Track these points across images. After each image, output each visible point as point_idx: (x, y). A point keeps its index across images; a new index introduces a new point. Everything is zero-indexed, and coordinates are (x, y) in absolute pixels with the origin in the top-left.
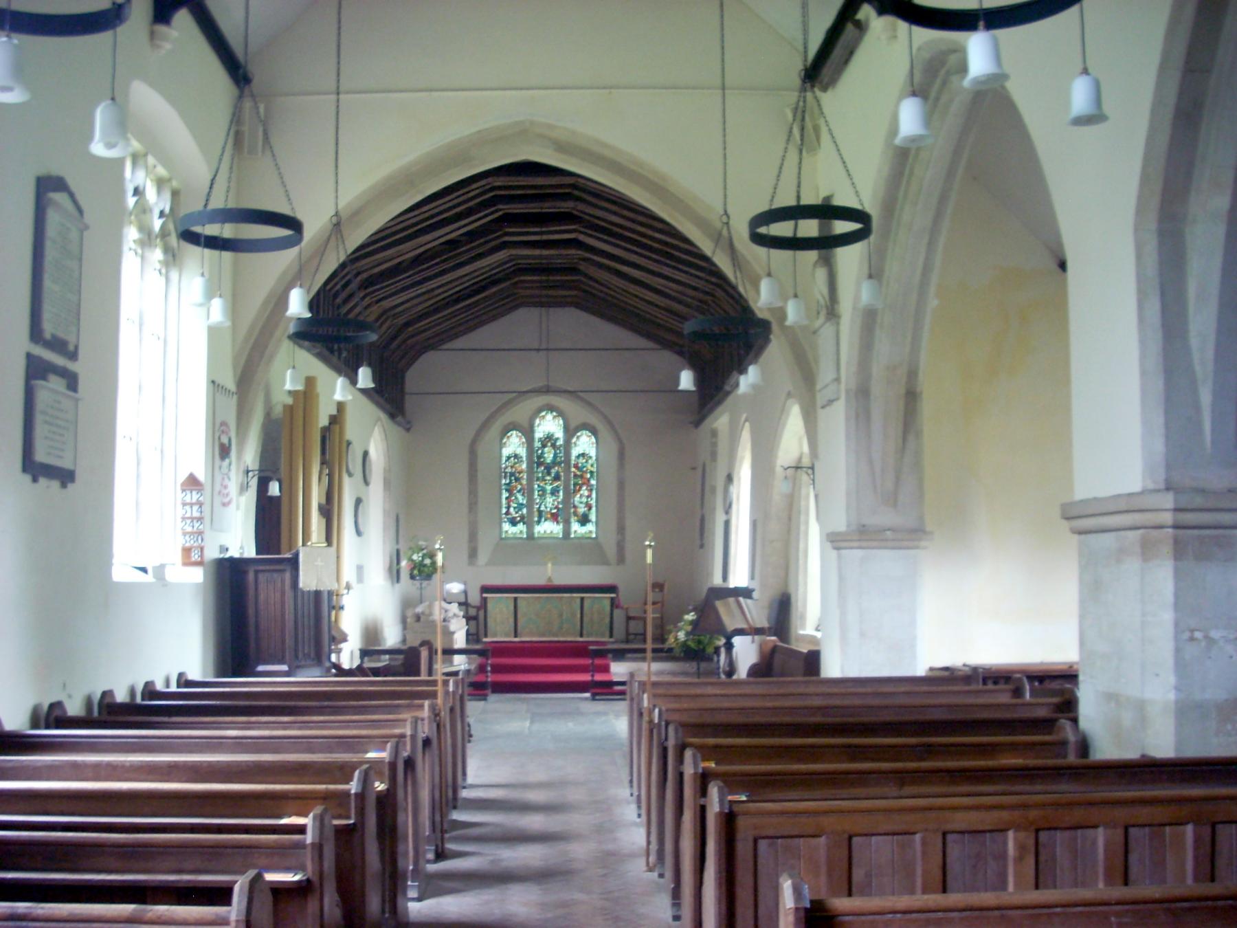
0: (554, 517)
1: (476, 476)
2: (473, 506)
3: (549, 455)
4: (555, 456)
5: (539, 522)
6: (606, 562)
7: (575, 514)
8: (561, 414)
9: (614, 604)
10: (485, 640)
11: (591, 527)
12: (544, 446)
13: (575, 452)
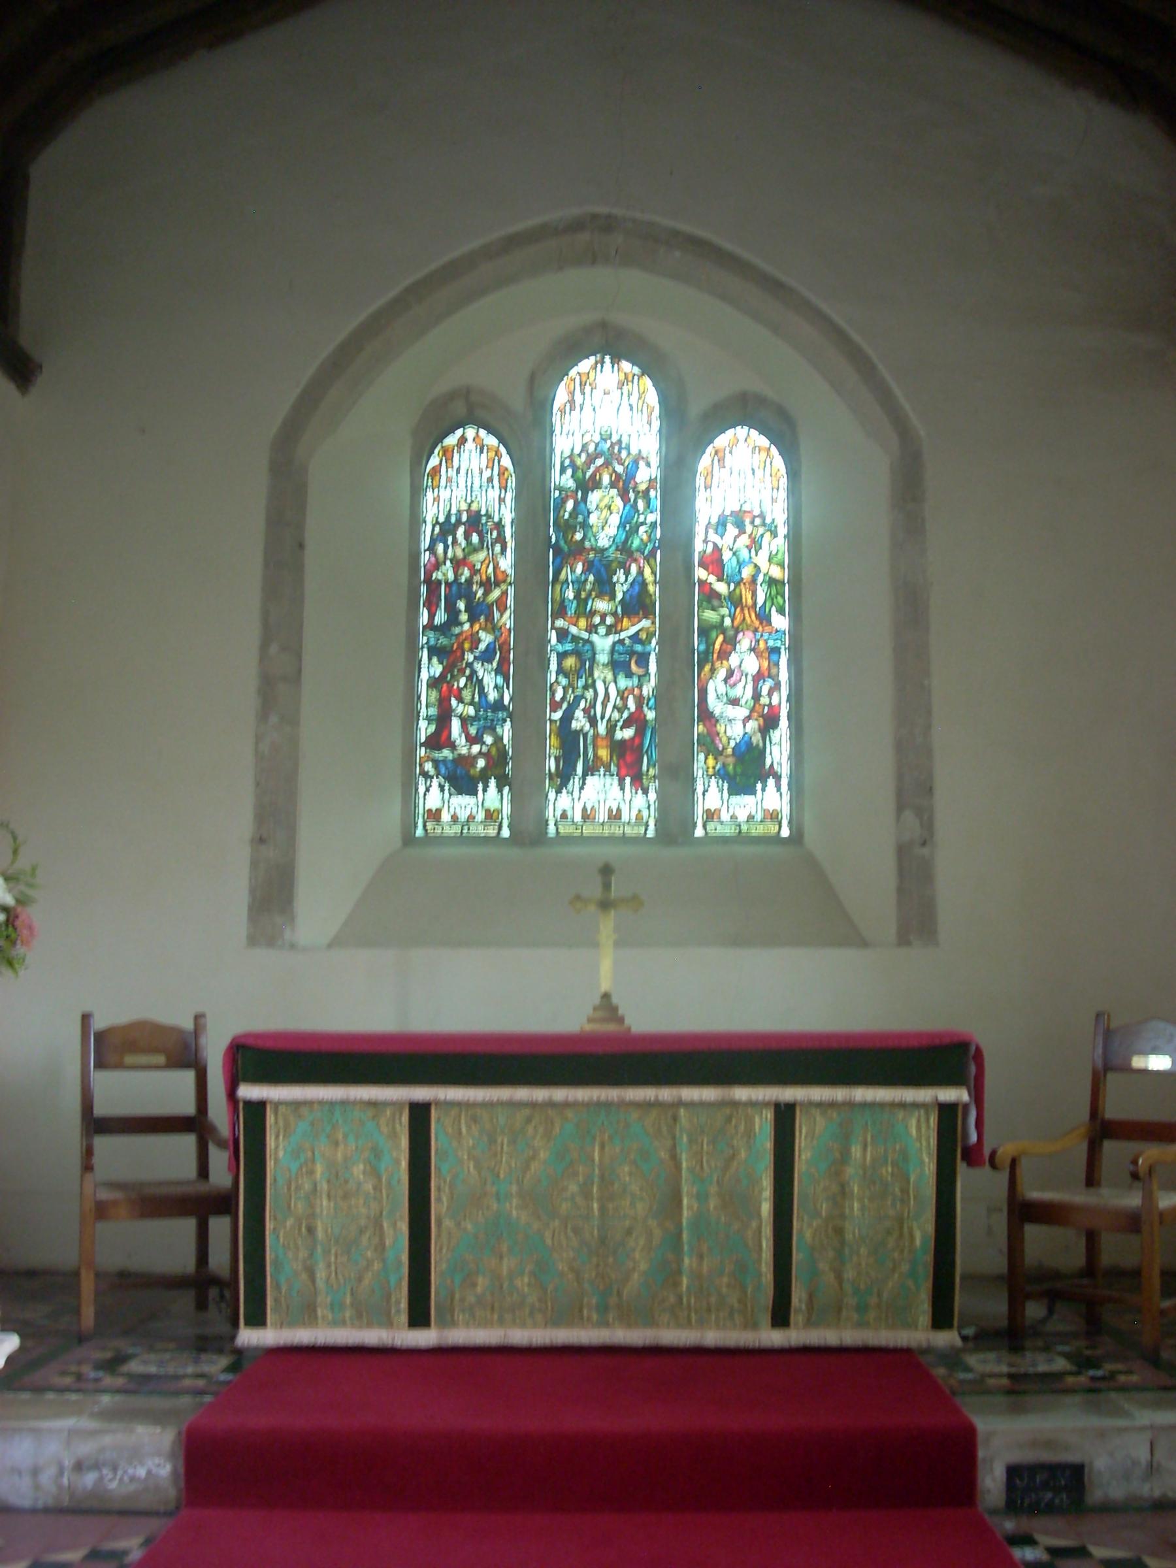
0: (627, 761)
1: (298, 568)
2: (278, 689)
3: (605, 519)
4: (629, 526)
5: (563, 778)
6: (850, 936)
7: (710, 744)
8: (652, 364)
9: (954, 1145)
10: (248, 1337)
11: (773, 798)
12: (587, 485)
13: (707, 507)
